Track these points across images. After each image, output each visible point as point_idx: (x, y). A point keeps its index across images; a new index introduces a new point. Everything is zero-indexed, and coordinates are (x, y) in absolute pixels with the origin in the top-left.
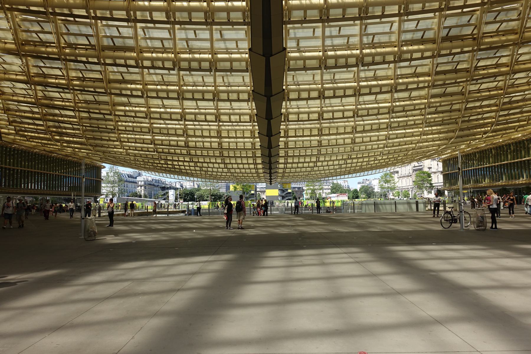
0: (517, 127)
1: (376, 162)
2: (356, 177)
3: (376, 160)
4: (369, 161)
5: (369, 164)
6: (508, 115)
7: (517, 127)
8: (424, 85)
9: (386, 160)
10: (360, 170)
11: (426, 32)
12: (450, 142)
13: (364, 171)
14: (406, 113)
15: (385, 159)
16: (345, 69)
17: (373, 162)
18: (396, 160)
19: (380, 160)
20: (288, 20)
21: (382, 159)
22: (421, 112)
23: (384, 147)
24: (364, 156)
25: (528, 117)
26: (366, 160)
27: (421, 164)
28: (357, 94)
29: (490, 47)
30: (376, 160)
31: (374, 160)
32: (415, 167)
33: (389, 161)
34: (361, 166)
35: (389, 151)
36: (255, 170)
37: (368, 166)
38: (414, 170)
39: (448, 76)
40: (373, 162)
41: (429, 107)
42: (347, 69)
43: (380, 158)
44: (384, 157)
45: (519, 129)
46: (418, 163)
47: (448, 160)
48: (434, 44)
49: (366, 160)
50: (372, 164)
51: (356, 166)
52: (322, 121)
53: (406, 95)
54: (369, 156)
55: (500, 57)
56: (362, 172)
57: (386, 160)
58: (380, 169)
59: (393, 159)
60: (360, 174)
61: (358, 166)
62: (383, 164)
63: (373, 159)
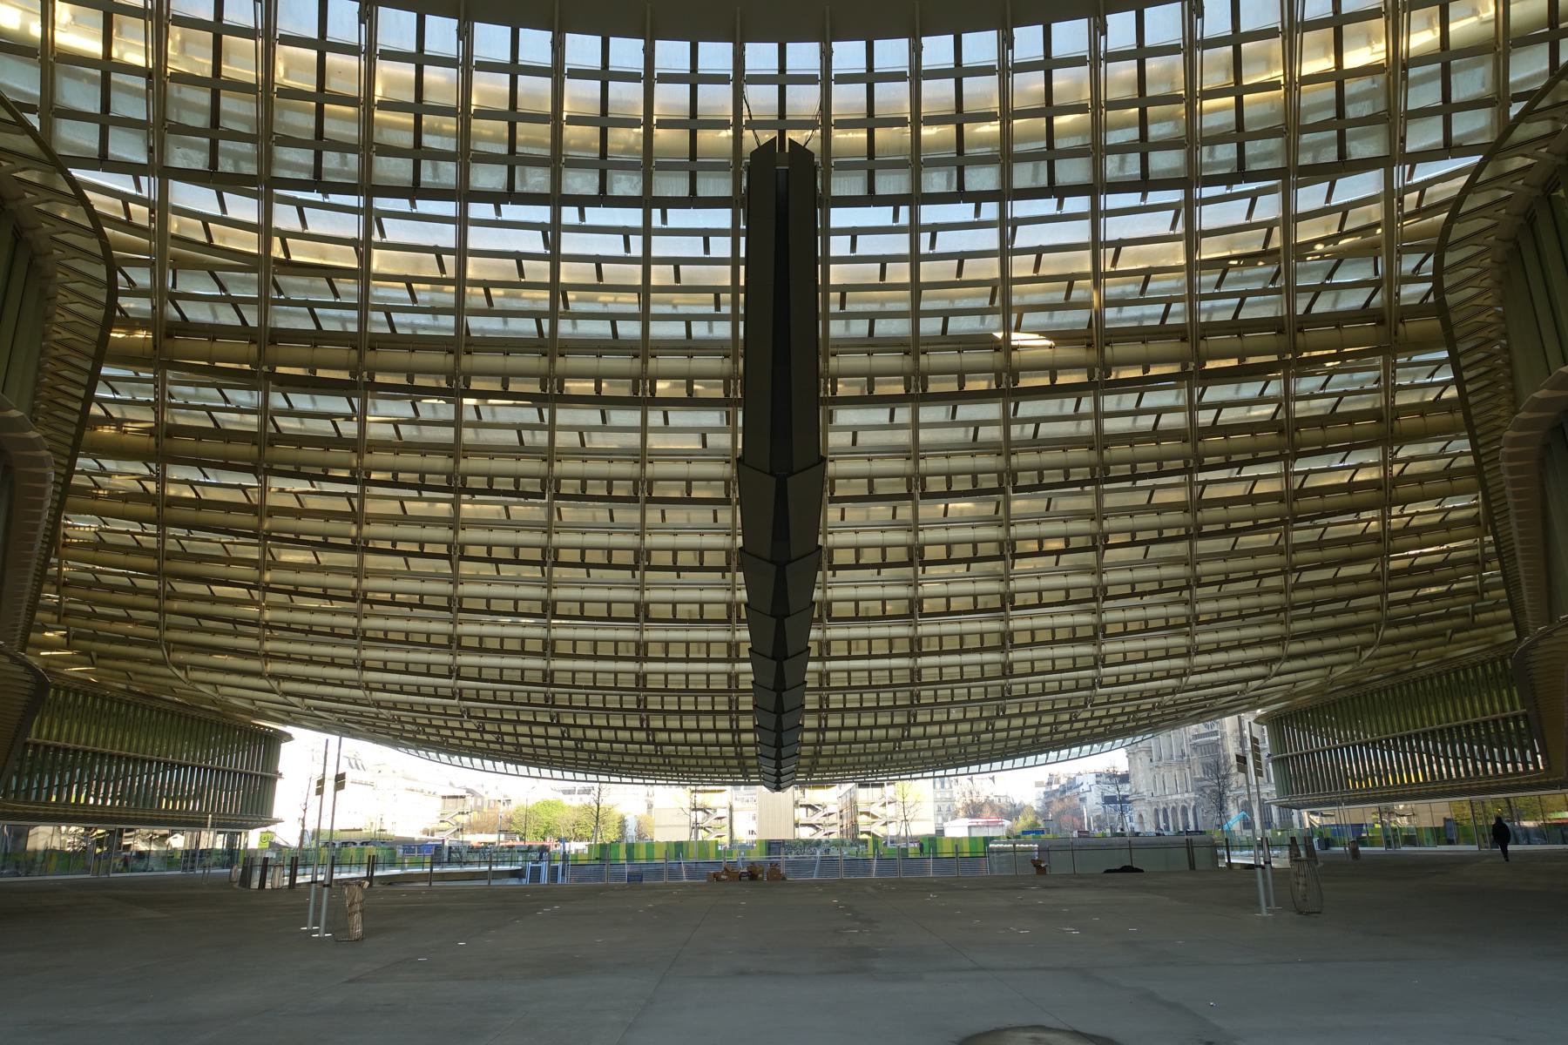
36: (733, 748)
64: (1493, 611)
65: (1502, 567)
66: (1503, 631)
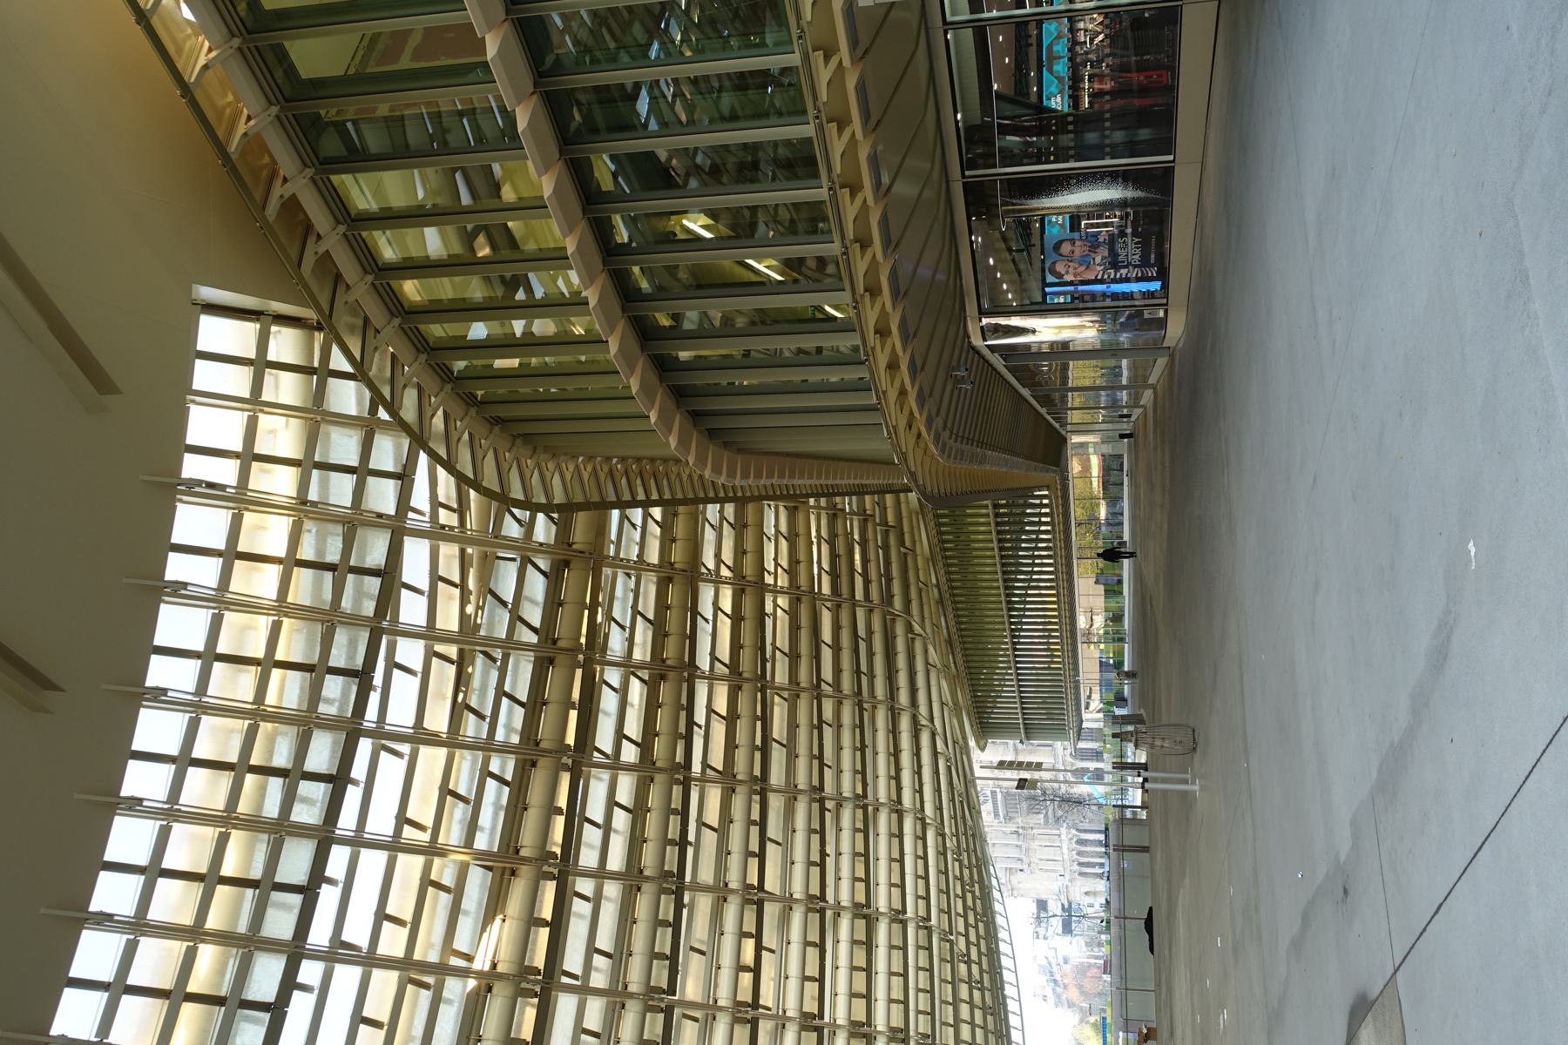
0: (902, 550)
1: (974, 956)
2: (1018, 986)
3: (969, 957)
4: (969, 983)
5: (981, 982)
6: (865, 575)
7: (902, 549)
8: (755, 802)
9: (971, 920)
10: (999, 1014)
11: (616, 800)
12: (922, 632)
13: (1004, 997)
14: (829, 811)
15: (967, 925)
16: (690, 851)
17: (975, 968)
18: (973, 886)
19: (968, 943)
20: (540, 978)
21: (966, 936)
22: (830, 767)
23: (926, 928)
24: (950, 979)
25: (878, 528)
26: (964, 994)
27: (989, 793)
28: (750, 1014)
29: (690, 638)
30: (968, 954)
31: (968, 963)
32: (996, 815)
33: (974, 909)
34: (983, 1008)
35: (941, 911)
37: (987, 983)
38: (1008, 818)
39: (741, 737)
40: (975, 968)
41: (819, 789)
42: (690, 844)
43: (962, 940)
44: (961, 929)
45: (908, 544)
46: (986, 801)
47: (981, 723)
48: (642, 889)
49: (964, 994)
50: (981, 971)
51: (985, 1028)
52: (827, 1019)
53: (778, 756)
54: (953, 983)
55: (717, 608)
56: (1005, 1005)
57: (971, 920)
58: (997, 940)
59: (969, 896)
60: (1006, 968)
61: (985, 1020)
62: (982, 932)
63: (963, 967)
64: (885, 508)
65: (843, 494)
66: (907, 502)
